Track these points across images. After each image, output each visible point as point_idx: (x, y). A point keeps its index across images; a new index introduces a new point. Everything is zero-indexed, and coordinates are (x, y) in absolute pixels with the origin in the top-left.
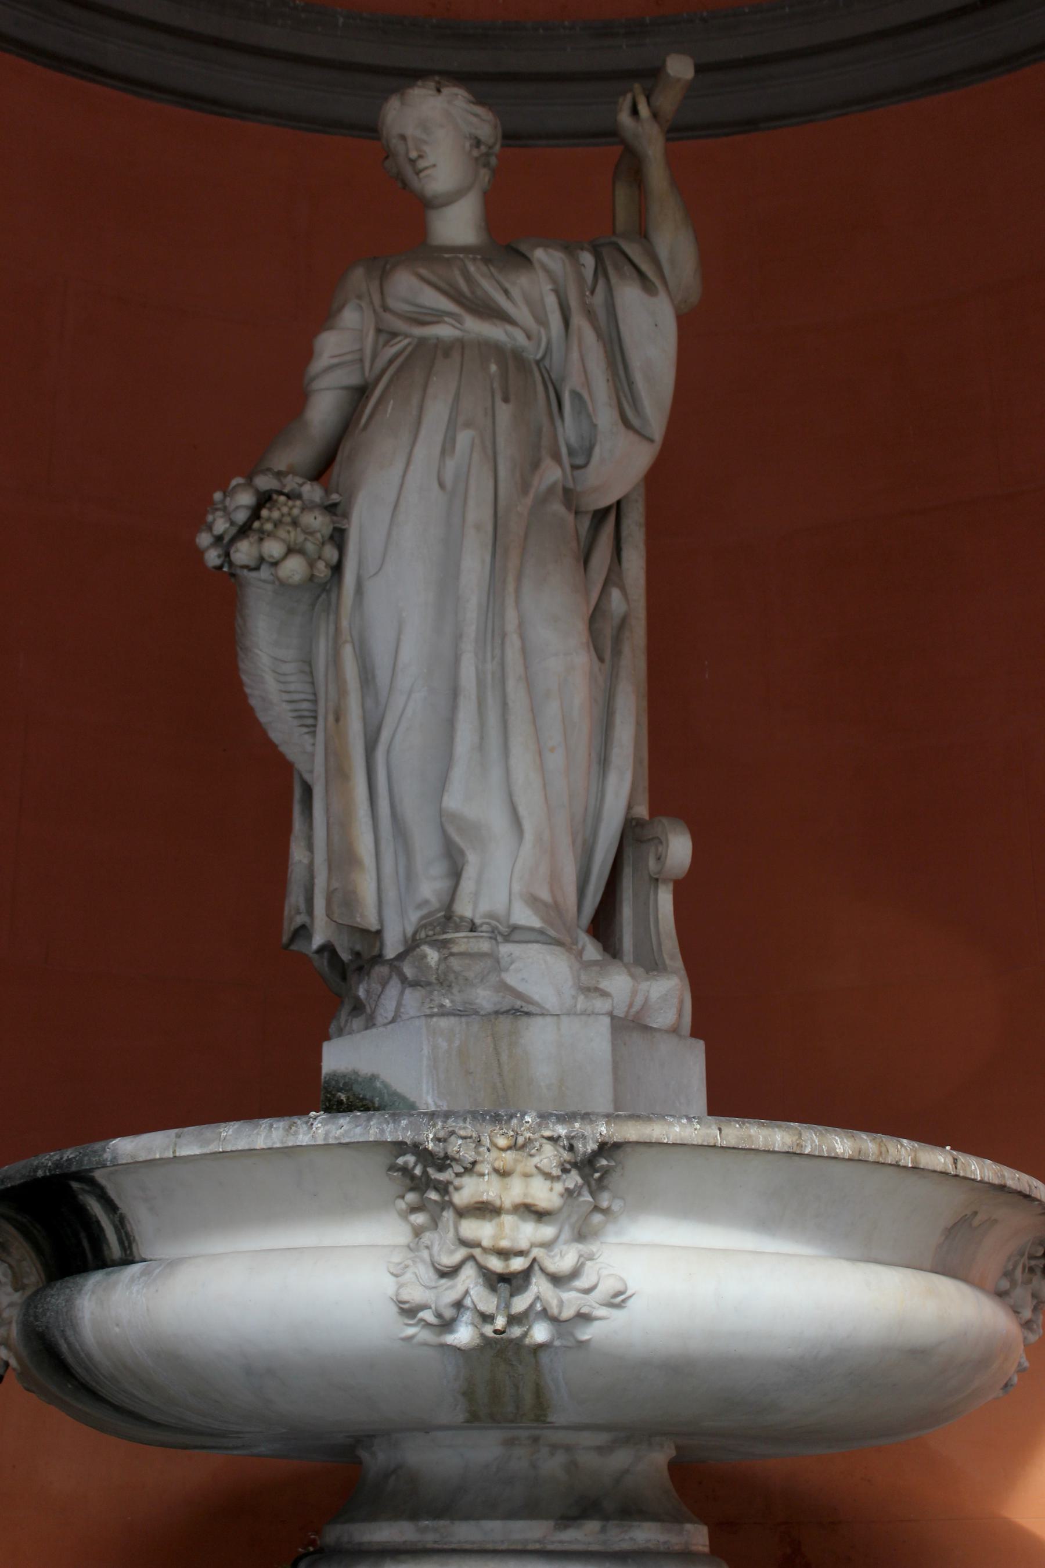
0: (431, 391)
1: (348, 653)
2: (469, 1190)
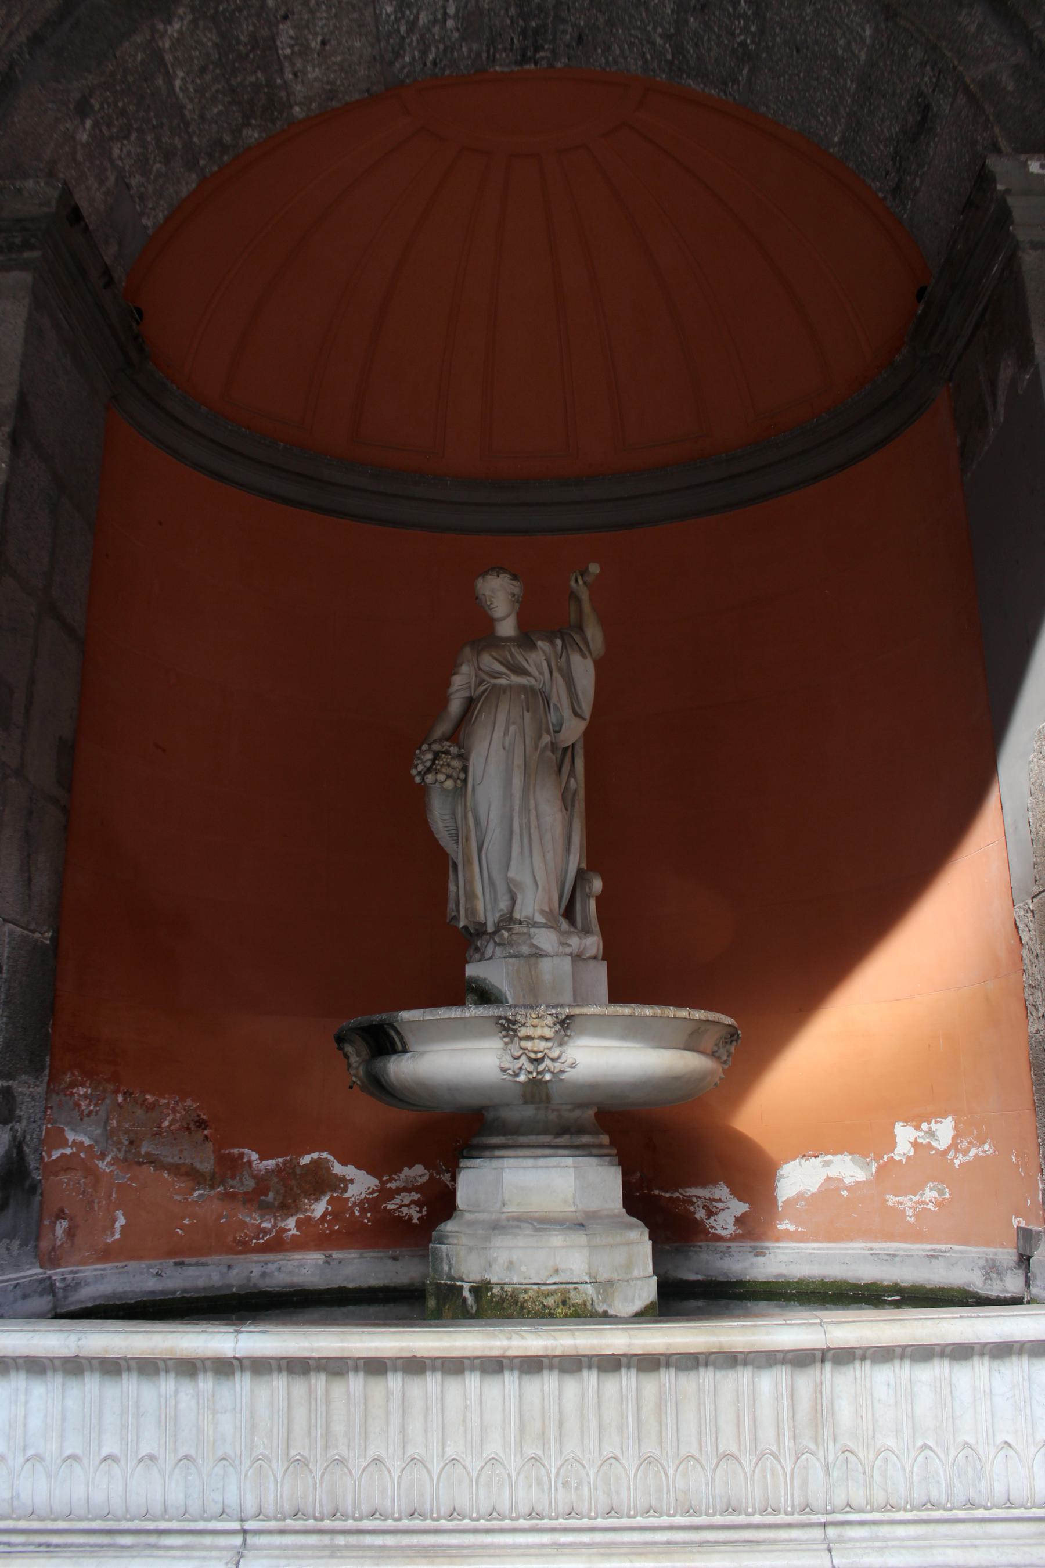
0: (499, 709)
1: (470, 815)
2: (523, 1032)
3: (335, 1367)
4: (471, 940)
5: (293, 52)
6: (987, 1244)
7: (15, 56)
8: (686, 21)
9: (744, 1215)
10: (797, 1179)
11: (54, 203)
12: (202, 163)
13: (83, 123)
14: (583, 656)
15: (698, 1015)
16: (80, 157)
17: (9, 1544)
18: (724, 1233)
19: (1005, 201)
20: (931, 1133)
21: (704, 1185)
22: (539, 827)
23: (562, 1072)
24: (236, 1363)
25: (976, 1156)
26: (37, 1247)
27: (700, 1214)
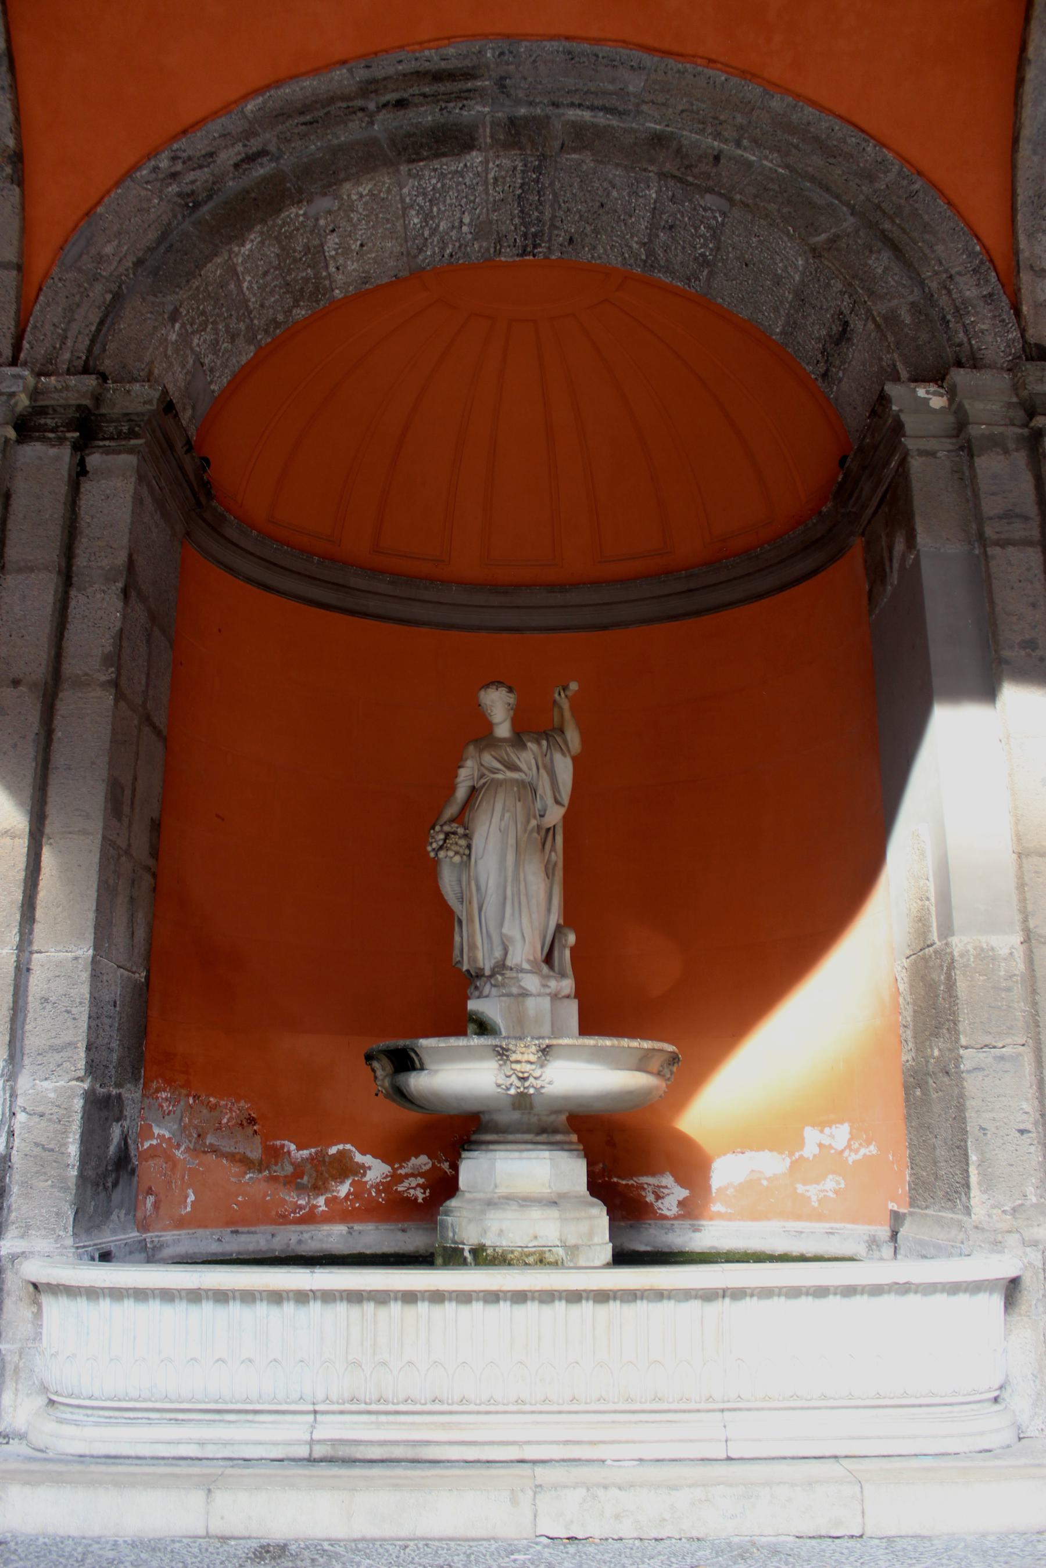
1: (473, 883)
2: (513, 1057)
3: (381, 1298)
4: (470, 980)
5: (337, 254)
6: (870, 1223)
7: (123, 278)
8: (658, 236)
9: (686, 1199)
10: (725, 1173)
11: (155, 402)
12: (259, 337)
13: (173, 327)
14: (563, 754)
15: (647, 1044)
16: (170, 353)
17: (149, 1419)
18: (668, 1213)
19: (899, 416)
20: (832, 1136)
21: (653, 1174)
22: (527, 895)
23: (542, 1087)
24: (311, 1294)
25: (865, 1155)
26: (135, 1216)
27: (650, 1198)
